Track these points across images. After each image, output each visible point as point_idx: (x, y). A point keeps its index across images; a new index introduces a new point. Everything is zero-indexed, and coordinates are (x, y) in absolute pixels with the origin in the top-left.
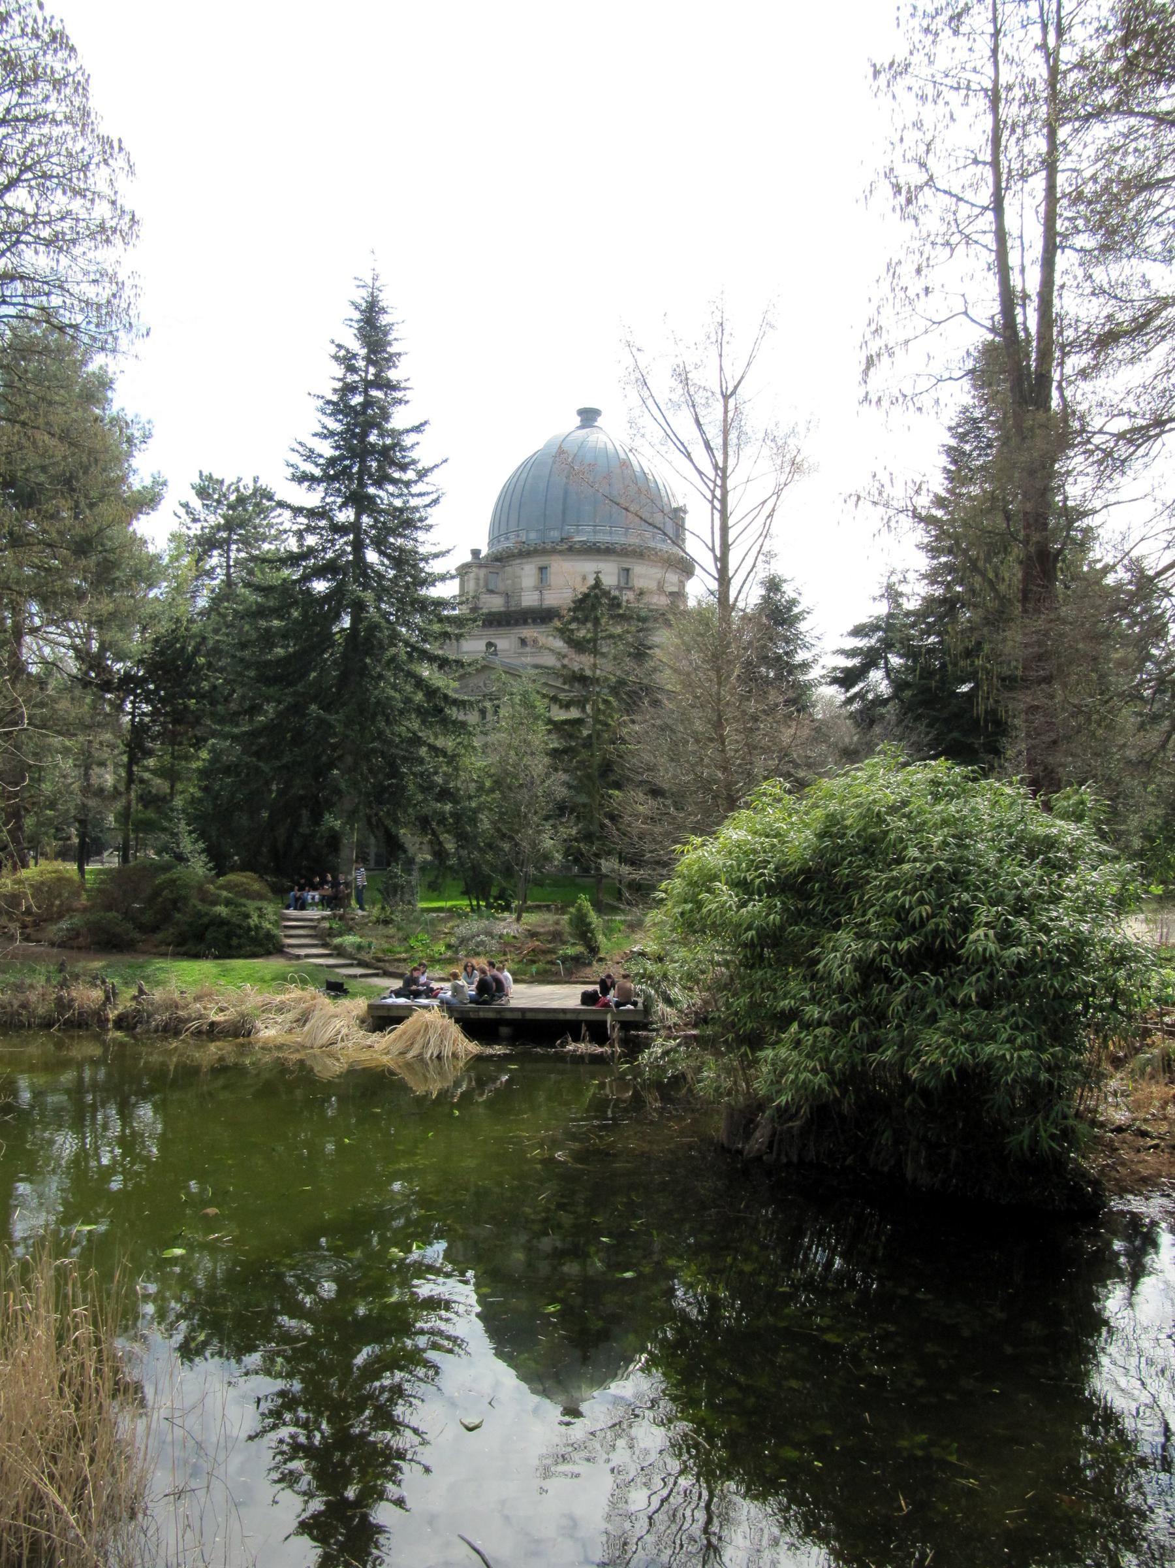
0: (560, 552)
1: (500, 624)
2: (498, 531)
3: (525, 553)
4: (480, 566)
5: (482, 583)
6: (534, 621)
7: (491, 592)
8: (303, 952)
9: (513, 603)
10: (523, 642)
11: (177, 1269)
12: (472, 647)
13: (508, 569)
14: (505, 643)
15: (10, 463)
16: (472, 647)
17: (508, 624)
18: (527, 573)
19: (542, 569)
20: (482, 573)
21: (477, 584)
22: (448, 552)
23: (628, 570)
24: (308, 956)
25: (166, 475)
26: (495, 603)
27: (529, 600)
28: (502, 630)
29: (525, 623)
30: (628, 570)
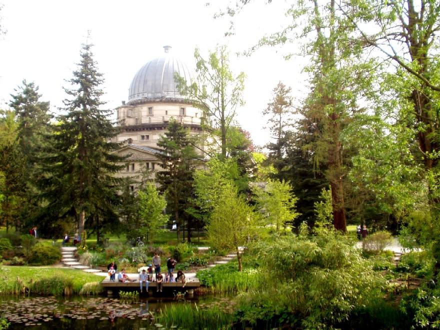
0: (158, 102)
1: (133, 130)
2: (133, 91)
3: (143, 103)
4: (125, 107)
5: (126, 114)
6: (147, 129)
7: (130, 117)
8: (69, 263)
9: (138, 122)
10: (143, 137)
11: (84, 155)
12: (121, 138)
13: (136, 109)
14: (136, 138)
15: (334, 136)
16: (121, 138)
17: (137, 130)
18: (144, 110)
19: (150, 109)
20: (126, 110)
21: (124, 114)
22: (106, 103)
23: (183, 109)
24: (73, 265)
25: (124, 100)
26: (130, 122)
27: (145, 121)
28: (134, 133)
29: (144, 129)
30: (183, 109)
